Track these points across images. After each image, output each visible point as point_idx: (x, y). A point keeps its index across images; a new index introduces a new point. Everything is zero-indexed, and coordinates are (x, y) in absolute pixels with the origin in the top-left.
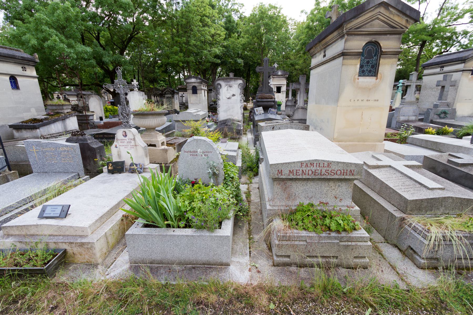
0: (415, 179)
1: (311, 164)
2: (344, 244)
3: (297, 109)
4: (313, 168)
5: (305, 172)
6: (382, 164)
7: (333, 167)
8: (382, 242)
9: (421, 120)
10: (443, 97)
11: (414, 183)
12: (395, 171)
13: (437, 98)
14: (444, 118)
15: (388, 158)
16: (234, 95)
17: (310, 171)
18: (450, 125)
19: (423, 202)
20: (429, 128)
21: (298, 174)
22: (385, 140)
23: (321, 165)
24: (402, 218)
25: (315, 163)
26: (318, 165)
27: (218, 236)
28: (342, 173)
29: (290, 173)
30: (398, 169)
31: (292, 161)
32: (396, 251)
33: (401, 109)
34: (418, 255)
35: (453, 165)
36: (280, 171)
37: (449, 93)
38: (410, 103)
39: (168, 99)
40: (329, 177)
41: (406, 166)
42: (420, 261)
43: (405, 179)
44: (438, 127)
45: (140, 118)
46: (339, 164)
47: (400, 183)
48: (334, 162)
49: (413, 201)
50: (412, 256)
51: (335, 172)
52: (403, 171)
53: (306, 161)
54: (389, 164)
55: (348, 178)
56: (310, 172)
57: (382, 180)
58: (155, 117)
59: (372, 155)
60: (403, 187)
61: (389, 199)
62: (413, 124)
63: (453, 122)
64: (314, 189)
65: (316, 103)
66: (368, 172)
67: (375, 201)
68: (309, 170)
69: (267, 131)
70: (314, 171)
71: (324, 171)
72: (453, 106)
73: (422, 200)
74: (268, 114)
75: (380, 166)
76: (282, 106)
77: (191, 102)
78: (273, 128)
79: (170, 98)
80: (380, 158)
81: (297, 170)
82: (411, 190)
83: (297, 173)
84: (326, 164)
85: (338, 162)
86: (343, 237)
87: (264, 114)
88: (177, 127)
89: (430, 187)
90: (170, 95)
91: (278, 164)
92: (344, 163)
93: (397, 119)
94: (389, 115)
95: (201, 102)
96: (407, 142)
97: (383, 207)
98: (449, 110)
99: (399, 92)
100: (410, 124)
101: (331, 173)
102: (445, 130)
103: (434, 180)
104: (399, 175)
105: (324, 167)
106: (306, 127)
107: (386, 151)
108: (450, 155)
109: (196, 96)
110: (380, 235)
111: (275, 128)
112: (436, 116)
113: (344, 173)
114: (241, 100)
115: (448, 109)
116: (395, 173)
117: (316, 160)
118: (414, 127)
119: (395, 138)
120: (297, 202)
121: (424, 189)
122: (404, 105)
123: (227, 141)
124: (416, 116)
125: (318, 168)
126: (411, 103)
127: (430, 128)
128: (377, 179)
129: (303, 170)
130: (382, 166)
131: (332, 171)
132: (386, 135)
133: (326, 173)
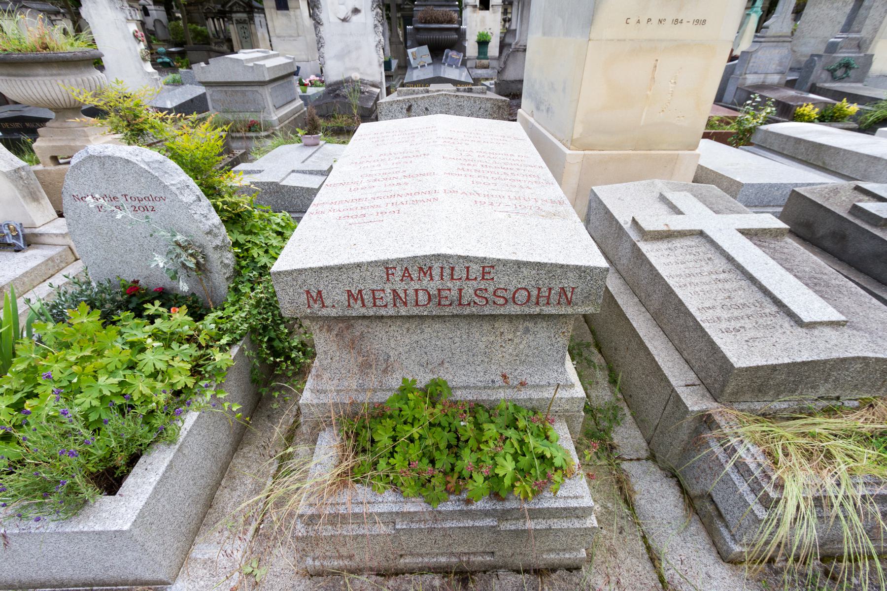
0: (764, 283)
1: (421, 269)
2: (513, 527)
3: (513, 52)
4: (432, 284)
5: (402, 295)
6: (679, 228)
7: (502, 280)
8: (638, 459)
9: (791, 84)
10: (855, 26)
11: (759, 295)
12: (713, 249)
13: (840, 27)
14: (841, 79)
15: (700, 206)
16: (356, 11)
17: (421, 293)
18: (853, 98)
19: (777, 373)
20: (805, 104)
21: (378, 303)
22: (706, 136)
23: (459, 272)
24: (703, 416)
25: (436, 265)
26: (447, 272)
27: (87, 533)
28: (534, 299)
29: (352, 301)
30: (720, 243)
31: (352, 261)
32: (669, 491)
33: (754, 56)
34: (727, 527)
35: (863, 220)
36: (314, 295)
37: (872, 12)
38: (777, 39)
39: (241, 26)
40: (487, 310)
41: (745, 233)
42: (728, 547)
43: (735, 283)
44: (826, 103)
45: (9, 75)
46: (523, 269)
47: (721, 296)
48: (505, 263)
49: (748, 369)
50: (711, 522)
51: (508, 295)
52: (733, 253)
53: (402, 260)
54: (697, 227)
55: (554, 312)
56: (422, 298)
57: (671, 282)
58: (54, 72)
59: (661, 195)
60: (725, 315)
61: (681, 342)
62: (773, 96)
63: (858, 88)
64: (447, 342)
65: (544, 34)
66: (639, 250)
67: (642, 343)
68: (416, 291)
69: (392, 118)
70: (434, 292)
71: (471, 291)
72: (867, 48)
73: (774, 368)
74: (443, 66)
75: (674, 231)
76: (490, 44)
77: (277, 31)
78: (409, 109)
79: (244, 22)
80: (679, 206)
81: (373, 291)
82: (748, 324)
83: (374, 298)
84: (475, 269)
85: (519, 264)
86: (508, 511)
87: (431, 67)
88: (212, 100)
89: (806, 318)
90: (244, 16)
91: (300, 271)
92: (539, 265)
93: (740, 81)
94: (727, 67)
95: (300, 33)
96: (751, 141)
97: (659, 368)
98: (858, 58)
99: (756, 12)
100: (766, 94)
101: (496, 299)
102: (841, 109)
103: (814, 284)
104: (720, 263)
105: (467, 278)
106: (499, 107)
107: (703, 176)
108: (858, 189)
109: (286, 15)
110: (638, 433)
111: (413, 109)
112: (825, 75)
113: (538, 296)
114: (376, 26)
115: (857, 55)
116: (710, 259)
117: (438, 257)
118: (777, 103)
119: (728, 129)
120: (395, 381)
121: (786, 323)
122: (764, 44)
123: (322, 143)
124: (782, 73)
125: (449, 285)
126: (779, 40)
127: (808, 105)
128: (658, 275)
129: (394, 291)
130: (679, 232)
131: (499, 293)
132: (709, 124)
133: (477, 300)
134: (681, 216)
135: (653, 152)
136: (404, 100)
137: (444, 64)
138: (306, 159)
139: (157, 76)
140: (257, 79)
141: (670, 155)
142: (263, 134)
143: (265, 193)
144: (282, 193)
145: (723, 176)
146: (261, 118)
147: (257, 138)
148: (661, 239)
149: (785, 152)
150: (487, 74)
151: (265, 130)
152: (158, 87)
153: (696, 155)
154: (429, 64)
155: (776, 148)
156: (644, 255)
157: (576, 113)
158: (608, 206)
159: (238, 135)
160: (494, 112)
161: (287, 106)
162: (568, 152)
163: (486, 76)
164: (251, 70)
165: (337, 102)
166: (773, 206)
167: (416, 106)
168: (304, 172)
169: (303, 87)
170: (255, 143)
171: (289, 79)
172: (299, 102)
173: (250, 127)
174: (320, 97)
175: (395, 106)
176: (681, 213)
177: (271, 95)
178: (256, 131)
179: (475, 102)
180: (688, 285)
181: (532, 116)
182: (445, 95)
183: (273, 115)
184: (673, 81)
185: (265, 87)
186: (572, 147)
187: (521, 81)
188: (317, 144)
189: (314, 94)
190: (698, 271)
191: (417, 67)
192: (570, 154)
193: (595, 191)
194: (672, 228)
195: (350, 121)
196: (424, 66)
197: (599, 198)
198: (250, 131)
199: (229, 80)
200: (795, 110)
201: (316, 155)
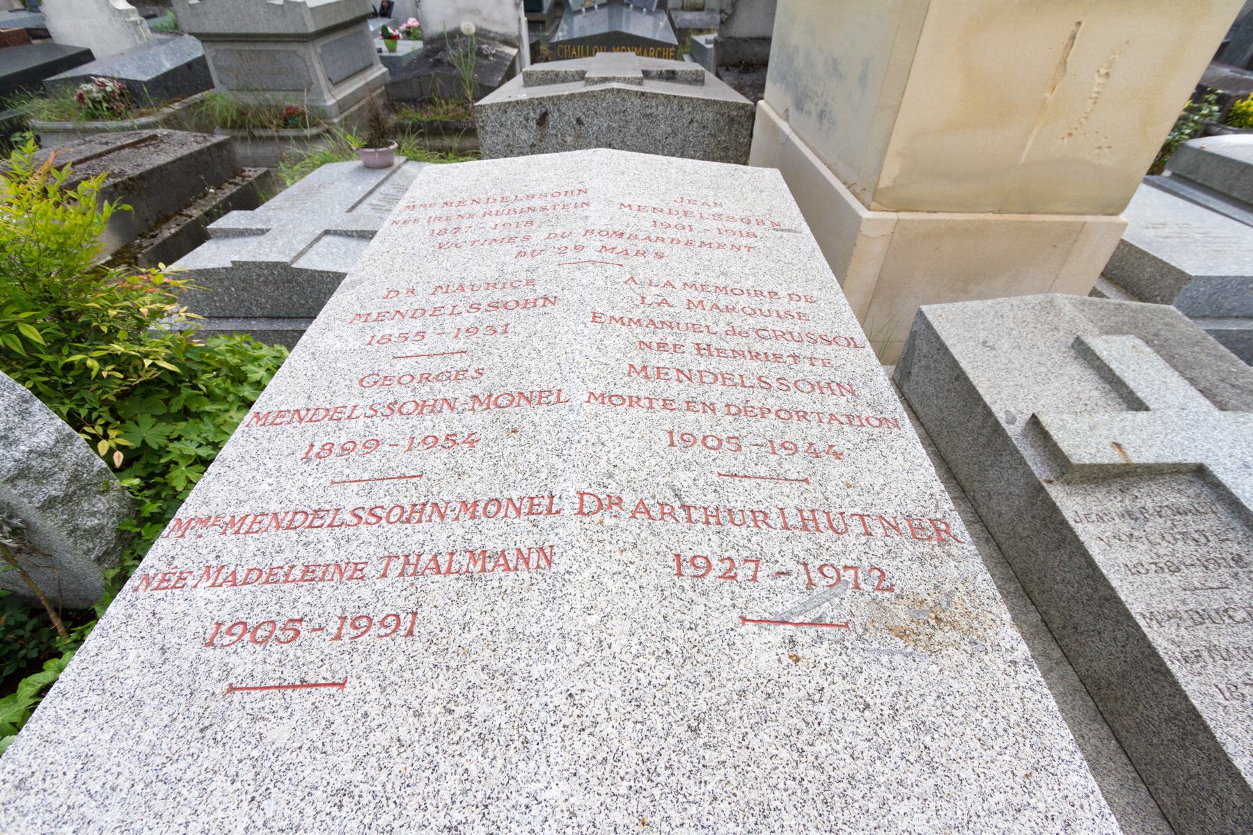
57: (1160, 639)
66: (1054, 509)
74: (625, 10)
87: (605, 10)
88: (218, 68)
106: (732, 120)
134: (1142, 415)
135: (1034, 218)
136: (531, 101)
137: (628, 5)
138: (360, 202)
139: (136, 17)
140: (292, 30)
141: (1068, 224)
142: (308, 132)
143: (266, 283)
144: (299, 284)
145: (1145, 253)
146: (302, 102)
147: (297, 138)
148: (1104, 479)
149: (1234, 194)
150: (701, 20)
151: (313, 125)
152: (140, 37)
153: (1119, 224)
154: (601, 6)
155: (1216, 186)
156: (1071, 529)
157: (890, 134)
158: (964, 365)
159: (263, 133)
160: (720, 131)
161: (357, 79)
162: (865, 214)
163: (699, 25)
164: (279, 13)
165: (437, 74)
166: (1237, 317)
167: (556, 115)
168: (347, 234)
169: (389, 41)
170: (294, 149)
171: (358, 28)
172: (380, 70)
173: (286, 120)
174: (411, 63)
175: (512, 114)
176: (1136, 404)
177: (322, 59)
178: (296, 127)
179: (681, 108)
180: (1205, 654)
181: (787, 120)
182: (619, 91)
183: (327, 96)
184: (1103, 71)
185: (310, 46)
186: (873, 204)
187: (766, 40)
188: (389, 165)
189: (408, 55)
190: (1217, 603)
191: (580, 12)
192: (868, 220)
193: (930, 317)
194: (1135, 459)
195: (461, 110)
196: (592, 8)
197: (938, 338)
198: (286, 126)
199: (243, 31)
200: (1233, 105)
201: (382, 189)
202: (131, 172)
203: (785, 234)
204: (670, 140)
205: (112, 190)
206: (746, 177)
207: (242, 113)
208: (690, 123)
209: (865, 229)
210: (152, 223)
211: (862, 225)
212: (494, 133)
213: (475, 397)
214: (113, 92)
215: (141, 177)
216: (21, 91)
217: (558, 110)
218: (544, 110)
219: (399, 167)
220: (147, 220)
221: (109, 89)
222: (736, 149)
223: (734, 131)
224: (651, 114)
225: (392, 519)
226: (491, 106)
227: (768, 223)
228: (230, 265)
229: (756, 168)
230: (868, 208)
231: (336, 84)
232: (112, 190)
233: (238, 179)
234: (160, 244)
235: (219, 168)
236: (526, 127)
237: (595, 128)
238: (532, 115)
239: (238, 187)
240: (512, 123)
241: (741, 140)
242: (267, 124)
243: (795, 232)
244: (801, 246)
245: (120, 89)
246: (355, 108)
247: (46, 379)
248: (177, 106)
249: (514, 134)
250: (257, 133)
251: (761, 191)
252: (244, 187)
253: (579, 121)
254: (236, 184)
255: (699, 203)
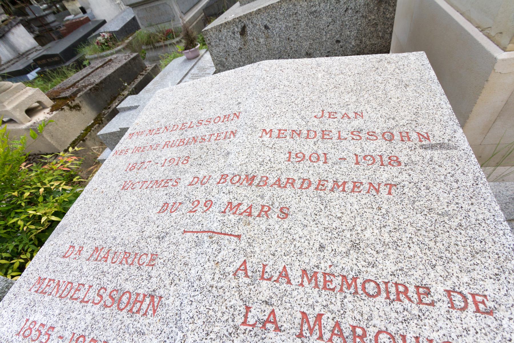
111: (248, 31)
151: (177, 36)
152: (121, 9)
160: (371, 12)
161: (195, 8)
162: (501, 55)
167: (251, 26)
188: (197, 56)
192: (503, 60)
201: (192, 71)
202: (98, 81)
203: (436, 154)
204: (331, 27)
205: (89, 92)
206: (391, 68)
207: (149, 37)
208: (346, 11)
209: (498, 68)
210: (109, 102)
211: (496, 65)
212: (216, 46)
213: (264, 130)
214: (108, 38)
215: (101, 82)
216: (81, 45)
217: (252, 22)
218: (243, 24)
219: (202, 56)
220: (106, 101)
221: (106, 37)
222: (384, 24)
223: (382, 9)
224: (315, 11)
225: (238, 177)
226: (211, 29)
227: (414, 136)
228: (119, 130)
229: (401, 55)
230: (504, 49)
231: (185, 14)
232: (89, 92)
233: (144, 73)
234: (112, 111)
235: (135, 69)
236: (234, 38)
237: (277, 30)
238: (236, 29)
239: (143, 76)
240: (225, 38)
241: (388, 16)
242: (160, 40)
243: (449, 147)
244: (458, 175)
245: (110, 36)
246: (195, 23)
247: (5, 231)
248: (130, 38)
249: (228, 44)
250: (157, 45)
251: (406, 86)
252: (146, 75)
253: (266, 27)
254: (143, 75)
255: (339, 116)
